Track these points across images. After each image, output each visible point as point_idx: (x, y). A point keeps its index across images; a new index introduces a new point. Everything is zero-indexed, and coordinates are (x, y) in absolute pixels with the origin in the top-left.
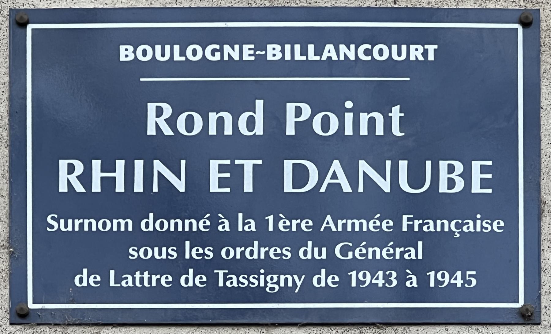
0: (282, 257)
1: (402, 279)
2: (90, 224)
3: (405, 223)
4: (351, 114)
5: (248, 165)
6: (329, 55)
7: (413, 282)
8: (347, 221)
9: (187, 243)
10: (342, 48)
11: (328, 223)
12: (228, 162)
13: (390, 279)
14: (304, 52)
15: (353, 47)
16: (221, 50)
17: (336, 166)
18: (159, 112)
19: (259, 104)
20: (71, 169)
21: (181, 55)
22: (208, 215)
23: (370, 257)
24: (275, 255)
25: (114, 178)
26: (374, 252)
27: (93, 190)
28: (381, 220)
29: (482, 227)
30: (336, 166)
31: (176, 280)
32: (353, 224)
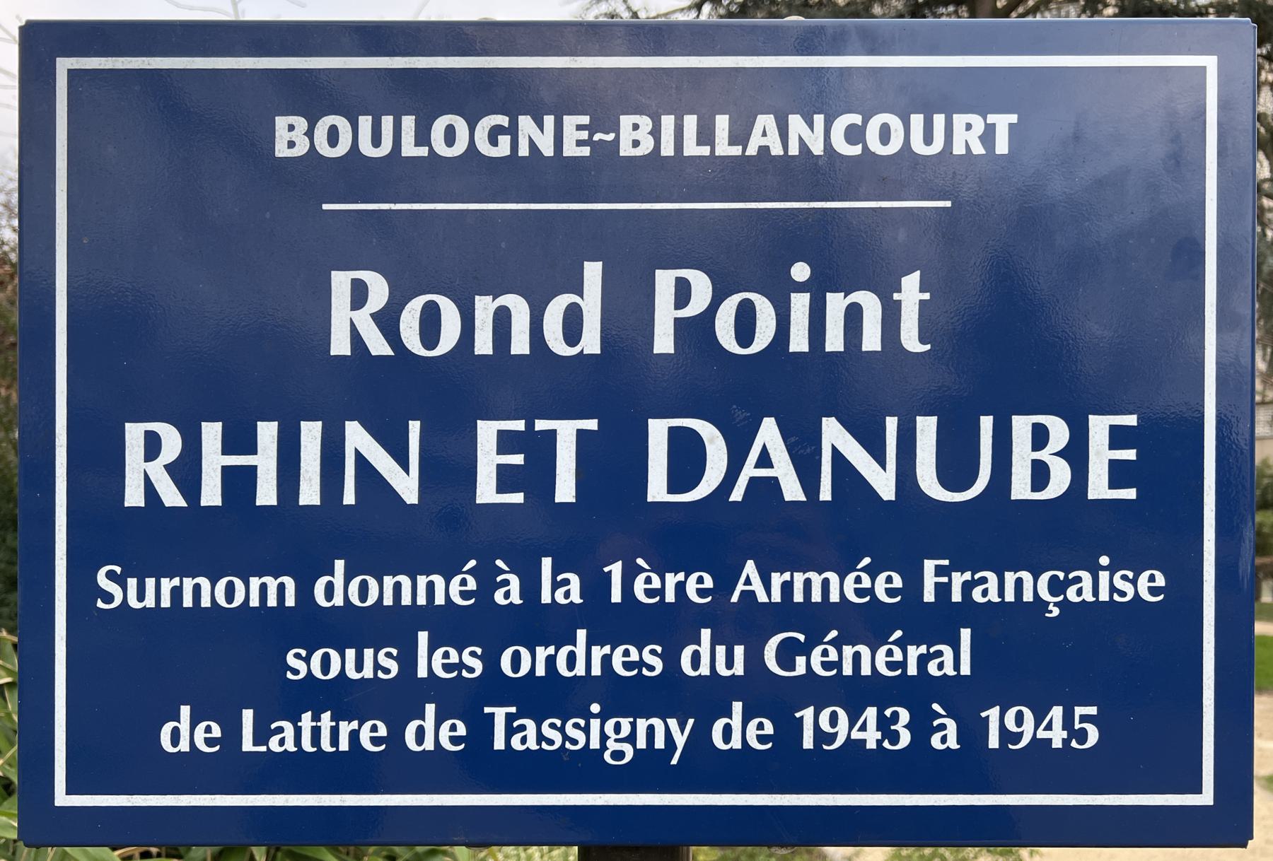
0: (460, 673)
1: (922, 727)
2: (197, 589)
3: (930, 580)
4: (807, 296)
5: (566, 432)
6: (764, 142)
7: (947, 737)
8: (792, 577)
9: (423, 637)
10: (796, 122)
11: (748, 582)
12: (519, 425)
13: (893, 728)
14: (706, 136)
15: (819, 119)
16: (513, 130)
17: (769, 433)
18: (359, 295)
19: (593, 272)
20: (153, 446)
21: (418, 143)
22: (472, 563)
23: (848, 670)
24: (627, 666)
25: (253, 469)
26: (857, 657)
27: (204, 502)
28: (873, 572)
29: (1113, 589)
30: (769, 433)
31: (396, 735)
32: (808, 583)
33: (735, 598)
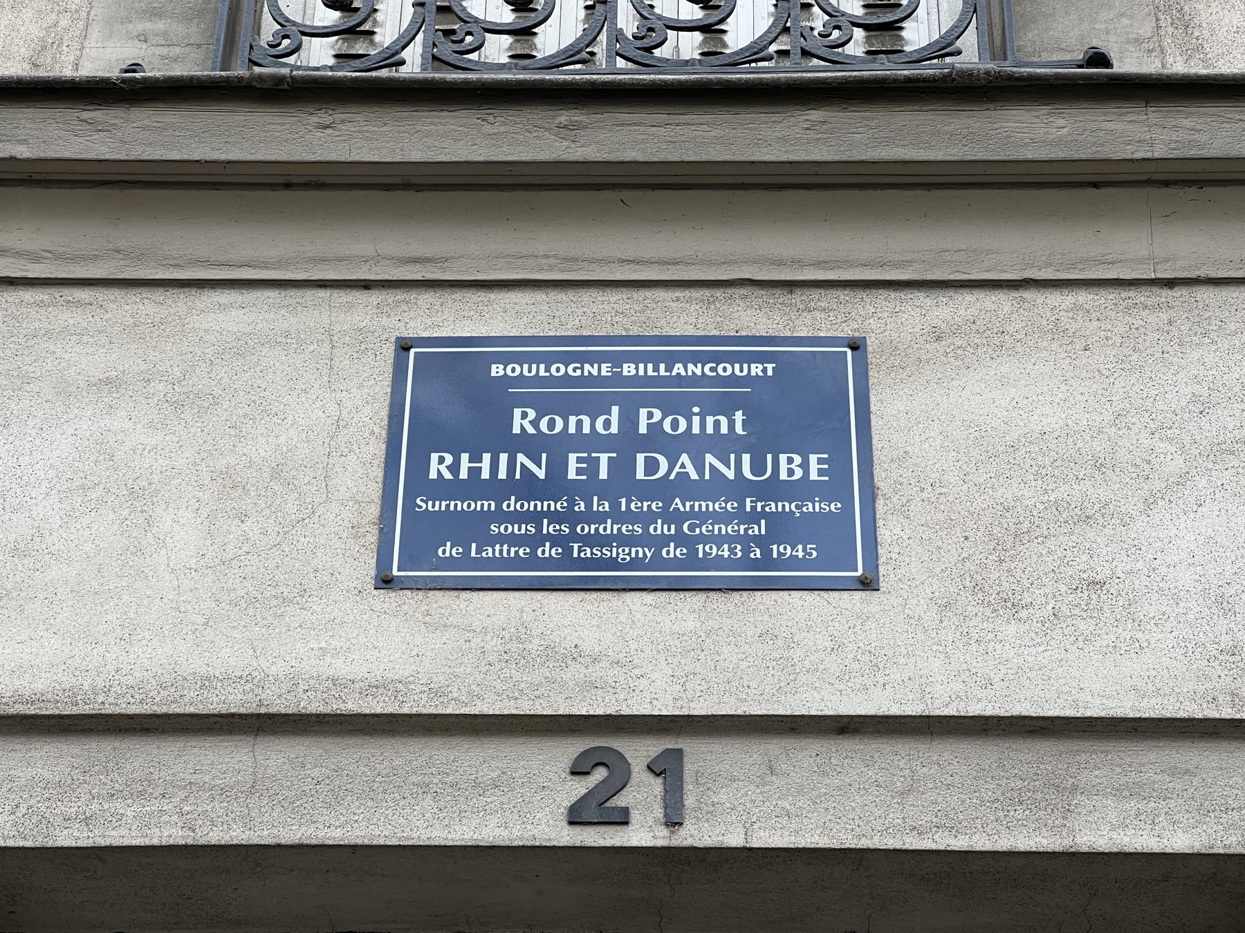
4: (698, 417)
5: (604, 458)
6: (679, 371)
9: (545, 521)
12: (586, 455)
16: (582, 368)
17: (684, 458)
29: (820, 508)
30: (684, 458)
33: (671, 510)
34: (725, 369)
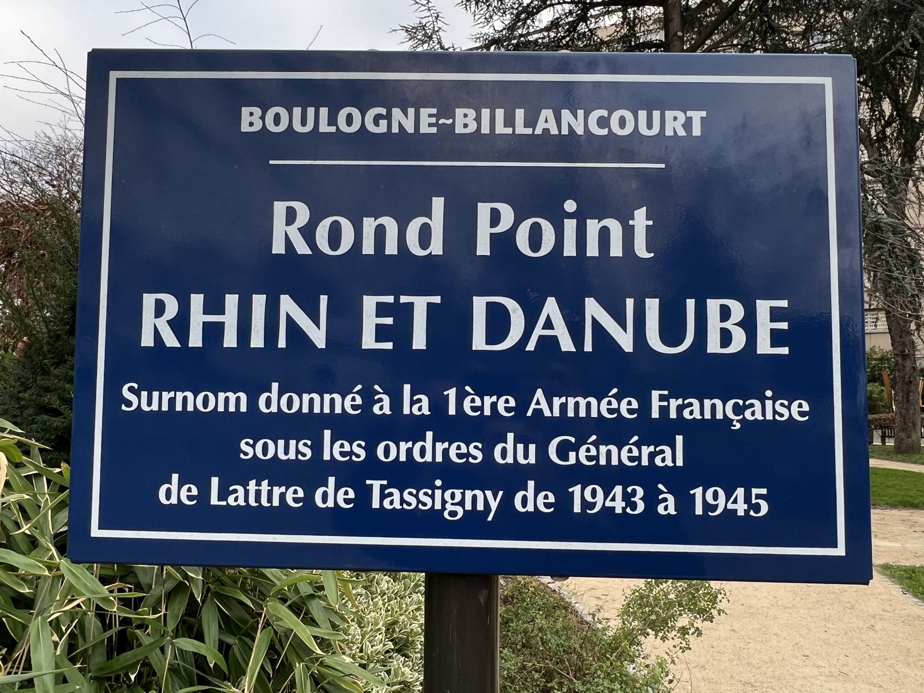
5: (420, 304)
6: (546, 126)
9: (327, 434)
16: (388, 117)
17: (551, 307)
33: (529, 414)
34: (622, 123)
